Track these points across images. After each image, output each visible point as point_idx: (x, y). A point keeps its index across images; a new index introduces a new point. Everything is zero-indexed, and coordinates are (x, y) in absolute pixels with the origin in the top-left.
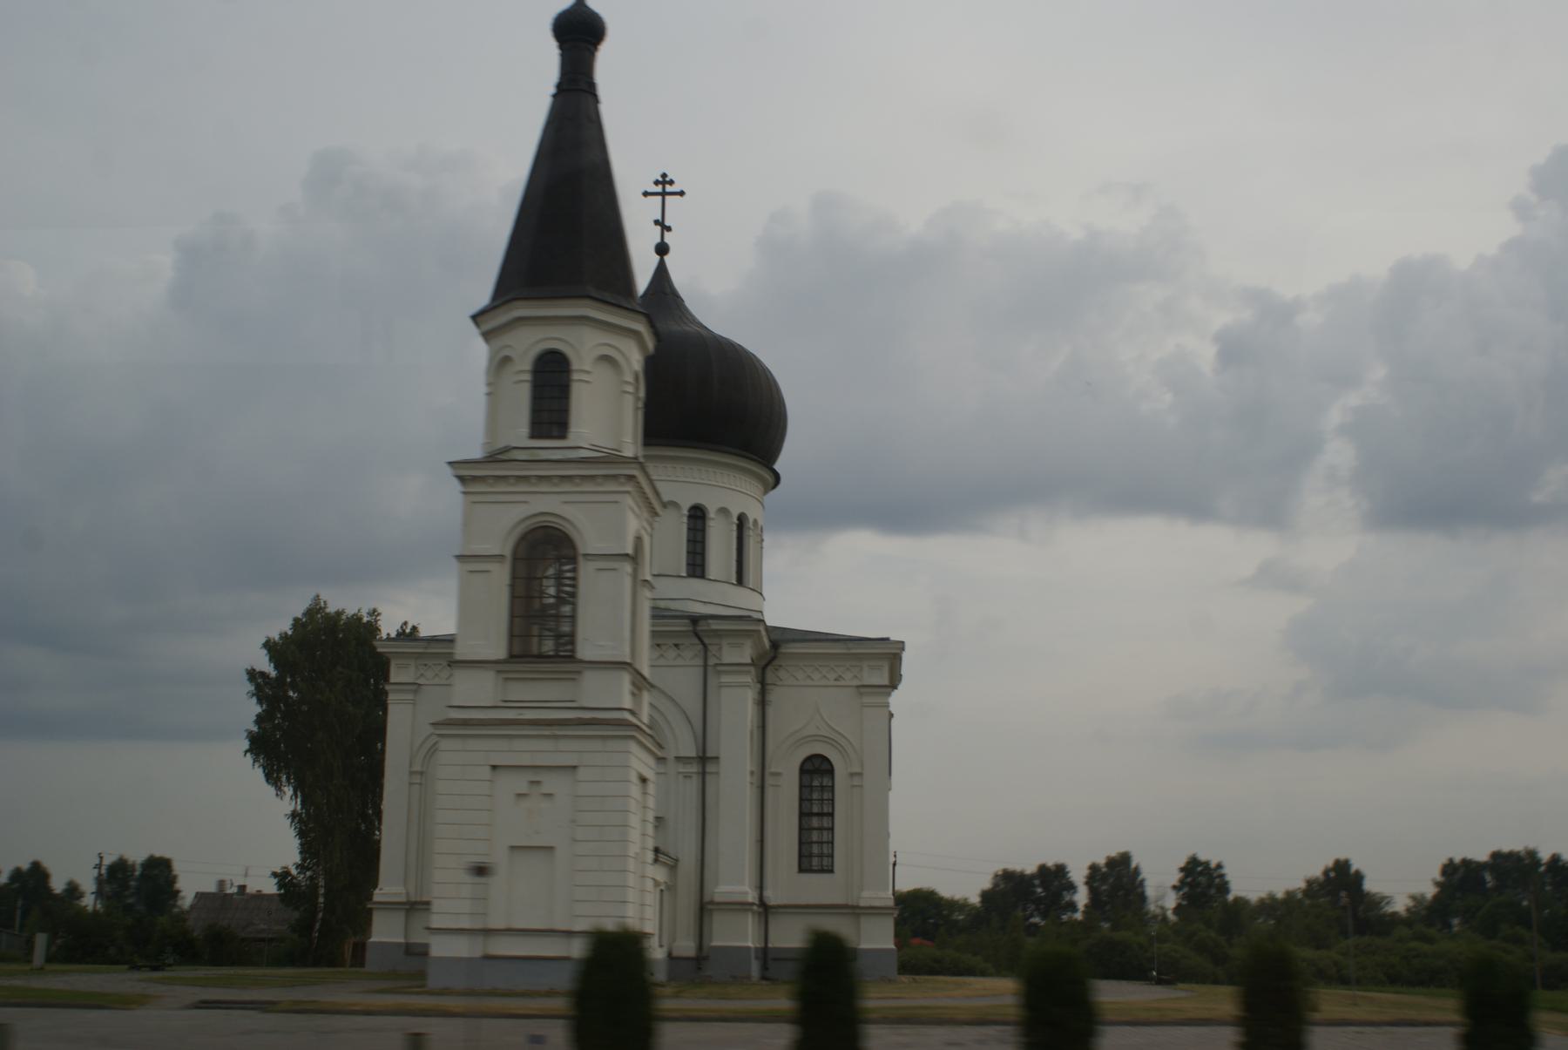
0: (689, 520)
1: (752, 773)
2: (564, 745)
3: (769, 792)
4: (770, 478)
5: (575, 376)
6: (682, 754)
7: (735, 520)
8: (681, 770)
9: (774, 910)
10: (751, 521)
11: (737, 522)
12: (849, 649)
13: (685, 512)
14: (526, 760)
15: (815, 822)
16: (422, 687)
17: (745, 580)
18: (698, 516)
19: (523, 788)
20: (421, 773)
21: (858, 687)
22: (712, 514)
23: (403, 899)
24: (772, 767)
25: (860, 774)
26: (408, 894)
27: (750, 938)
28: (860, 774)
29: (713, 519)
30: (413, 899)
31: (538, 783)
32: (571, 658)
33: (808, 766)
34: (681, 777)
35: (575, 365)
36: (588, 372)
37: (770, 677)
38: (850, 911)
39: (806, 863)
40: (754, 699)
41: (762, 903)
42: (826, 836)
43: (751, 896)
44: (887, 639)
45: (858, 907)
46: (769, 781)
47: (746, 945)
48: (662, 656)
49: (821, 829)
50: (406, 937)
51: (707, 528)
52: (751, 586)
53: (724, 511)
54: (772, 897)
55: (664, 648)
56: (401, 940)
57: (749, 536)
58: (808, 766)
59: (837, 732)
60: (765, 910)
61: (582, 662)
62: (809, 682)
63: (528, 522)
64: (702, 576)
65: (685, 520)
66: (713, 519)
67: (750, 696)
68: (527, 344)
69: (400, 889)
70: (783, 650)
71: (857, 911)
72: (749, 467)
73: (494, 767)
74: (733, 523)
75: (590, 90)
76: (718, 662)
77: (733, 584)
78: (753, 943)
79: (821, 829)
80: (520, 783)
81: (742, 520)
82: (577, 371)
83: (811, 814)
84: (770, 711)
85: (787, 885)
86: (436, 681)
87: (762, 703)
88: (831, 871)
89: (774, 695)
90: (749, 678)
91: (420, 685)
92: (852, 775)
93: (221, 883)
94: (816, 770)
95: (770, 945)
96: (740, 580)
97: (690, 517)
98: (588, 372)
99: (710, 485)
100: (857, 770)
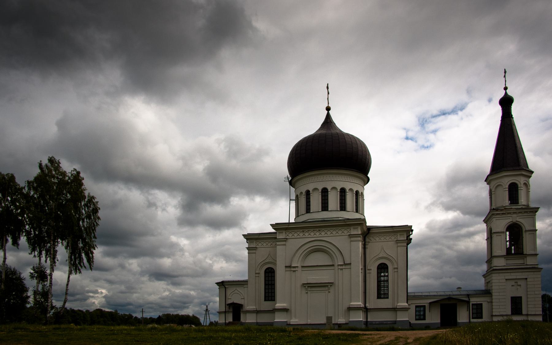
0: (340, 193)
1: (362, 269)
2: (512, 274)
3: (368, 275)
5: (519, 188)
9: (369, 310)
10: (360, 193)
13: (339, 190)
14: (515, 277)
16: (258, 248)
17: (359, 210)
18: (343, 192)
19: (514, 284)
20: (259, 273)
21: (349, 235)
23: (255, 310)
24: (368, 267)
25: (397, 268)
26: (256, 308)
27: (362, 318)
28: (397, 268)
29: (348, 192)
30: (258, 310)
31: (517, 282)
32: (522, 253)
34: (339, 270)
35: (519, 186)
36: (522, 187)
37: (367, 240)
39: (379, 296)
40: (362, 247)
43: (362, 305)
45: (397, 308)
46: (367, 272)
47: (360, 320)
48: (304, 234)
50: (256, 320)
51: (346, 195)
52: (361, 213)
53: (351, 190)
55: (305, 232)
56: (255, 321)
59: (389, 255)
60: (366, 310)
61: (526, 254)
62: (380, 240)
63: (510, 223)
66: (348, 192)
67: (360, 244)
68: (506, 182)
70: (370, 231)
71: (396, 309)
72: (355, 174)
73: (506, 279)
74: (354, 193)
75: (511, 116)
77: (354, 212)
80: (513, 283)
82: (520, 187)
84: (368, 251)
85: (373, 302)
87: (364, 248)
88: (388, 298)
89: (368, 246)
91: (257, 248)
92: (395, 268)
94: (382, 268)
96: (357, 211)
97: (340, 192)
98: (522, 187)
99: (343, 181)
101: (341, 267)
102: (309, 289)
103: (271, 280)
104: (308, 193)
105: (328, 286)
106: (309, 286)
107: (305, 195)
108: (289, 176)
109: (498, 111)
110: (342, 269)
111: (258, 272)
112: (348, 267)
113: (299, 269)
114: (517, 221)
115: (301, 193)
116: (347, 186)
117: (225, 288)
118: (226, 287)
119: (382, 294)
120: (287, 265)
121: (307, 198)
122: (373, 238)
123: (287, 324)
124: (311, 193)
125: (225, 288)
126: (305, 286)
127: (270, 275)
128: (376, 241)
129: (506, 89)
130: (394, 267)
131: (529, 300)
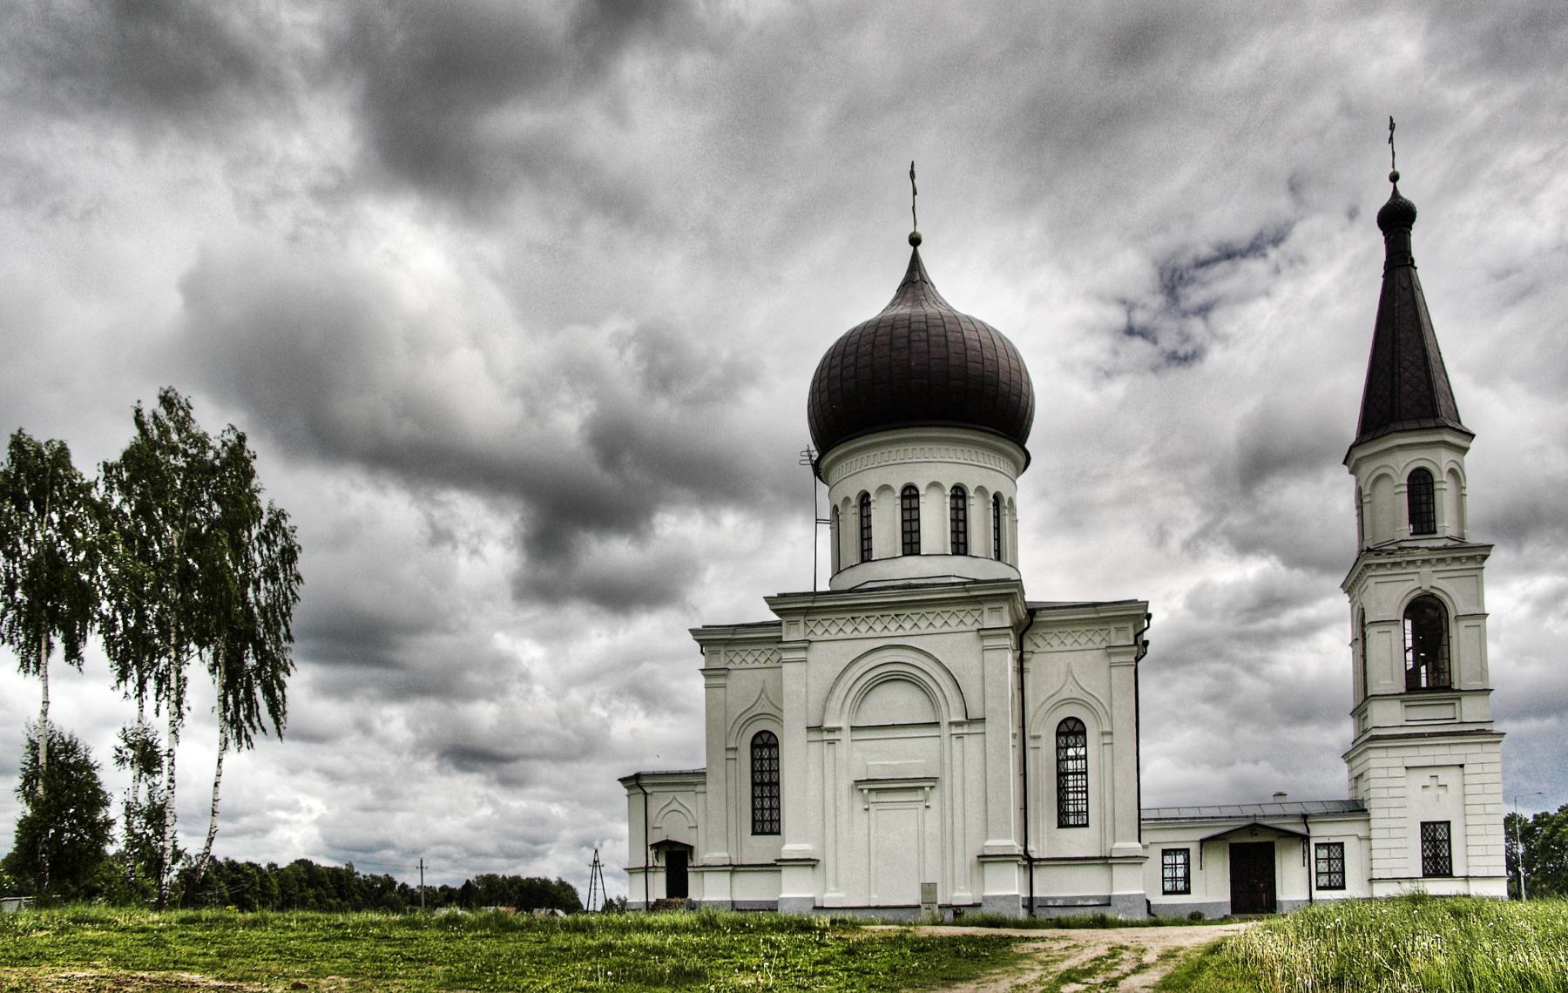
3: (1030, 754)
4: (1022, 460)
6: (953, 719)
7: (991, 498)
8: (825, 738)
9: (1037, 863)
11: (993, 500)
12: (1098, 613)
13: (948, 492)
15: (1071, 765)
18: (959, 493)
22: (971, 493)
28: (1111, 733)
29: (973, 498)
30: (735, 863)
33: (1064, 729)
34: (954, 737)
37: (1028, 646)
38: (1102, 862)
40: (1014, 667)
41: (1027, 856)
42: (1080, 764)
44: (1135, 601)
46: (1030, 743)
49: (1076, 758)
50: (731, 896)
52: (1008, 562)
53: (981, 490)
54: (1035, 851)
56: (729, 899)
57: (1005, 515)
58: (1064, 729)
60: (1030, 863)
62: (1062, 648)
64: (965, 554)
65: (948, 499)
66: (973, 498)
67: (1009, 659)
69: (725, 854)
70: (1035, 619)
76: (981, 627)
77: (991, 559)
78: (1019, 891)
79: (1076, 758)
81: (997, 498)
83: (1068, 759)
84: (1029, 678)
86: (744, 665)
87: (1021, 671)
90: (1010, 642)
92: (1103, 734)
93: (12, 436)
95: (1034, 895)
100: (1108, 729)
101: (959, 731)
102: (873, 797)
103: (770, 771)
104: (865, 500)
105: (923, 788)
106: (872, 787)
107: (856, 507)
108: (812, 447)
109: (1376, 243)
110: (960, 736)
111: (734, 746)
112: (977, 728)
113: (845, 736)
114: (1432, 587)
115: (847, 500)
116: (971, 482)
117: (646, 794)
118: (648, 790)
119: (766, 820)
120: (812, 724)
121: (862, 517)
122: (1058, 637)
123: (815, 908)
124: (873, 501)
125: (646, 794)
126: (862, 790)
127: (766, 753)
128: (1052, 649)
129: (1394, 178)
130: (1101, 730)
131: (1469, 800)
